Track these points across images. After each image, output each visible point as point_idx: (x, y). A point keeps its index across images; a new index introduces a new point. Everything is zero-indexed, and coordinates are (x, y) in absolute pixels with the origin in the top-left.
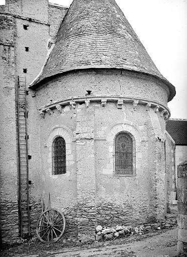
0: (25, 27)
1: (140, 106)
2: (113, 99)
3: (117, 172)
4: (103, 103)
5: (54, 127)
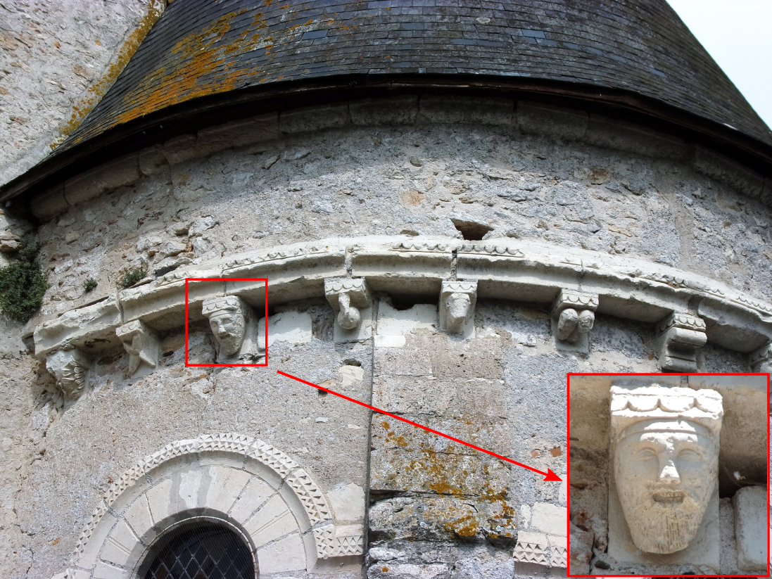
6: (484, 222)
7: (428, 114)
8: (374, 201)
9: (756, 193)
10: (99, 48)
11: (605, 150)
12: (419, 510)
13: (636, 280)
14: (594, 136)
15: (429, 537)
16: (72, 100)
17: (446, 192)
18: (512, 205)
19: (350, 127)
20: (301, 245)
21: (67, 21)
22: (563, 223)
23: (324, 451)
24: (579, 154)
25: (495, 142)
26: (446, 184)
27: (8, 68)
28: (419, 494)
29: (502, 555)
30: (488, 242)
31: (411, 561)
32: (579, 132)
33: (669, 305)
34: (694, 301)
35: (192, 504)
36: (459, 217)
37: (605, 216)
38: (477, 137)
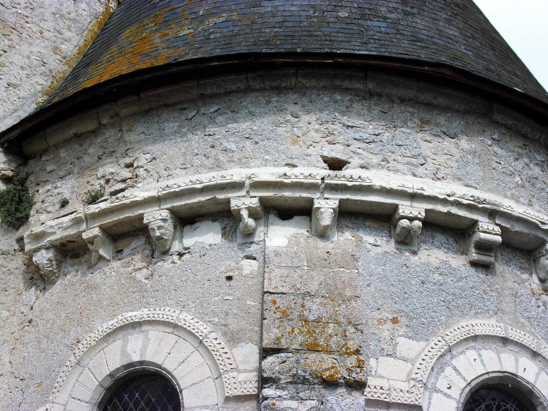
6: (344, 158)
7: (304, 81)
8: (266, 142)
9: (537, 137)
11: (429, 106)
12: (298, 362)
13: (451, 199)
14: (422, 97)
16: (51, 71)
17: (317, 136)
21: (48, 15)
22: (400, 159)
24: (411, 109)
25: (351, 101)
26: (317, 131)
28: (297, 350)
29: (356, 394)
30: (347, 172)
31: (292, 398)
32: (411, 94)
33: (475, 217)
35: (136, 358)
36: (326, 154)
37: (429, 154)
38: (339, 97)
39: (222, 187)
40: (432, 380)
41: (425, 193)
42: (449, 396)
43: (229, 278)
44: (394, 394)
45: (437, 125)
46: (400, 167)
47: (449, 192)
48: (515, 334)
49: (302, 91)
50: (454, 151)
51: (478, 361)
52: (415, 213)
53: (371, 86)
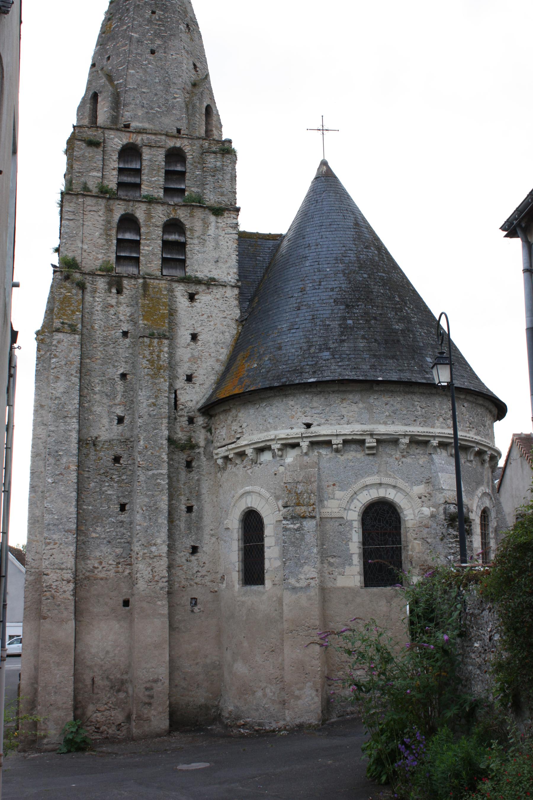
0: (192, 297)
1: (414, 446)
2: (355, 437)
3: (192, 506)
4: (334, 446)
5: (241, 491)
6: (311, 422)
7: (294, 391)
8: (282, 419)
9: (398, 390)
10: (223, 350)
11: (344, 392)
12: (293, 511)
13: (353, 433)
14: (341, 389)
15: (295, 517)
16: (217, 372)
17: (299, 414)
18: (318, 415)
19: (275, 396)
20: (266, 434)
21: (212, 345)
22: (333, 418)
23: (276, 491)
24: (337, 395)
25: (313, 397)
26: (300, 412)
27: (196, 369)
28: (293, 506)
29: (313, 520)
30: (312, 429)
31: (292, 524)
32: (336, 389)
33: (364, 438)
34: (372, 435)
35: (249, 506)
36: (304, 422)
37: (345, 413)
38: (307, 396)
39: (268, 440)
40: (348, 506)
41: (341, 433)
42: (355, 511)
43: (276, 474)
44: (333, 514)
45: (349, 399)
46: (333, 422)
47: (351, 430)
48: (385, 480)
49: (294, 395)
50: (356, 409)
51: (368, 495)
52: (338, 442)
53: (319, 389)
